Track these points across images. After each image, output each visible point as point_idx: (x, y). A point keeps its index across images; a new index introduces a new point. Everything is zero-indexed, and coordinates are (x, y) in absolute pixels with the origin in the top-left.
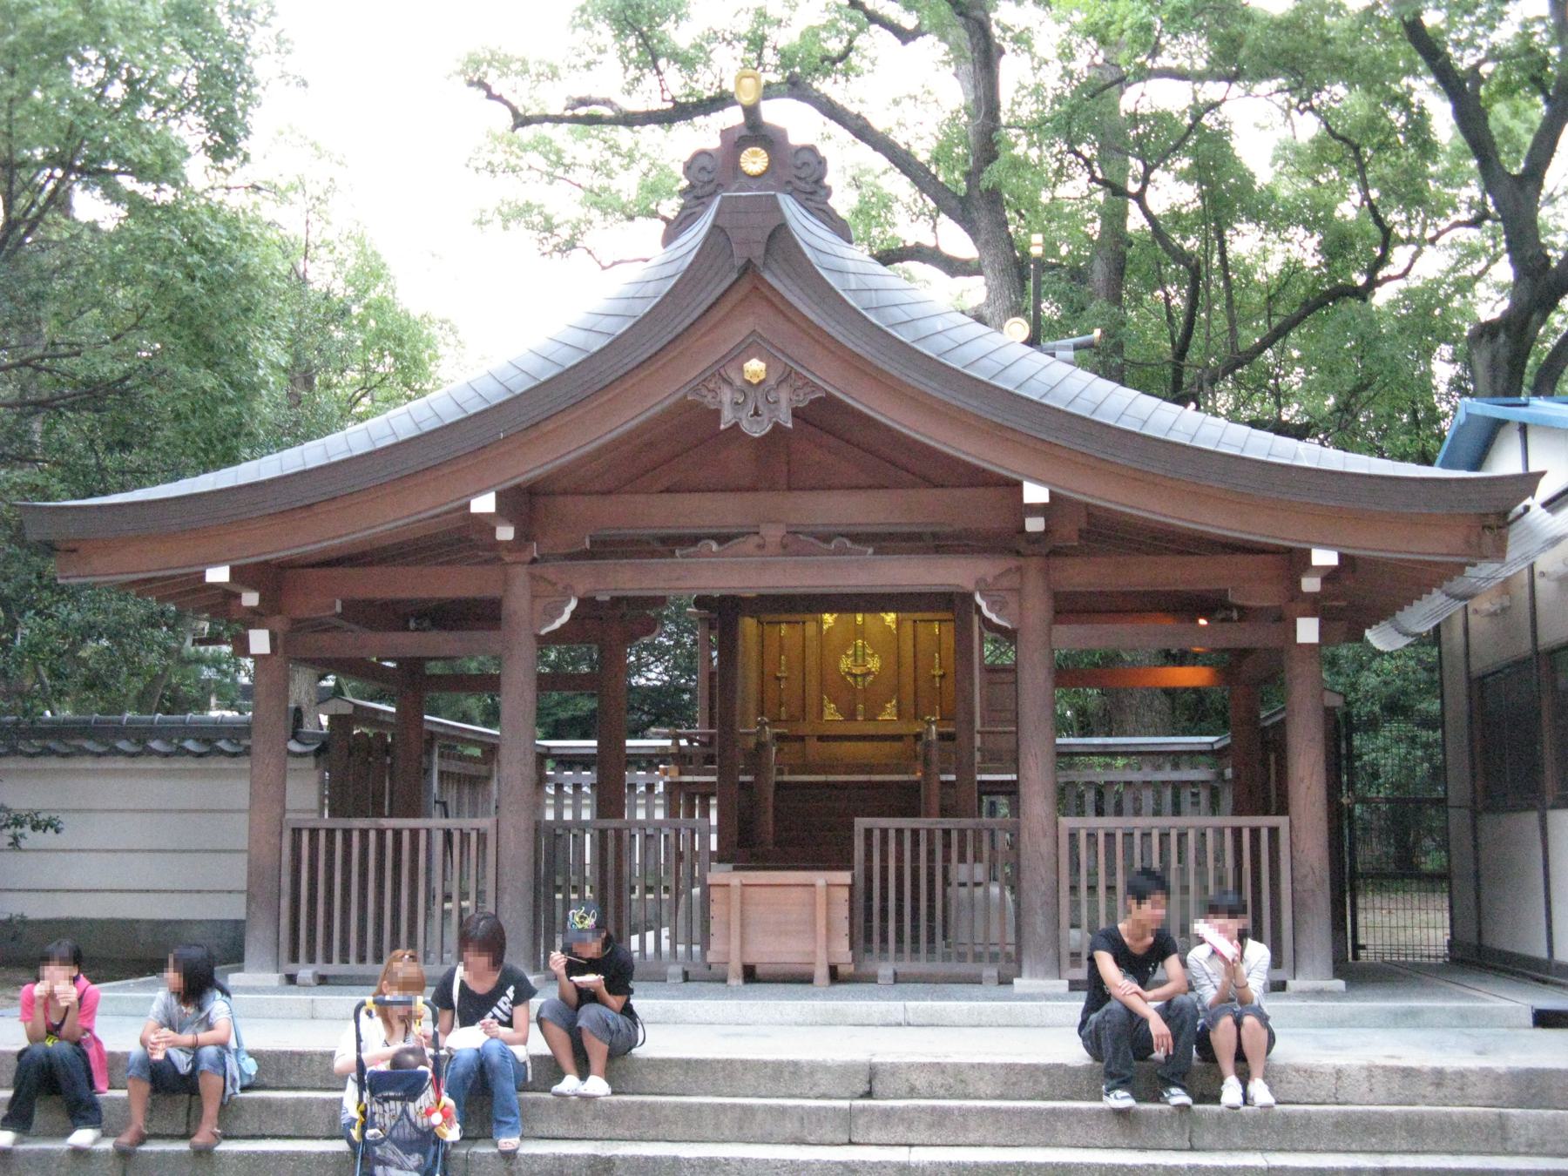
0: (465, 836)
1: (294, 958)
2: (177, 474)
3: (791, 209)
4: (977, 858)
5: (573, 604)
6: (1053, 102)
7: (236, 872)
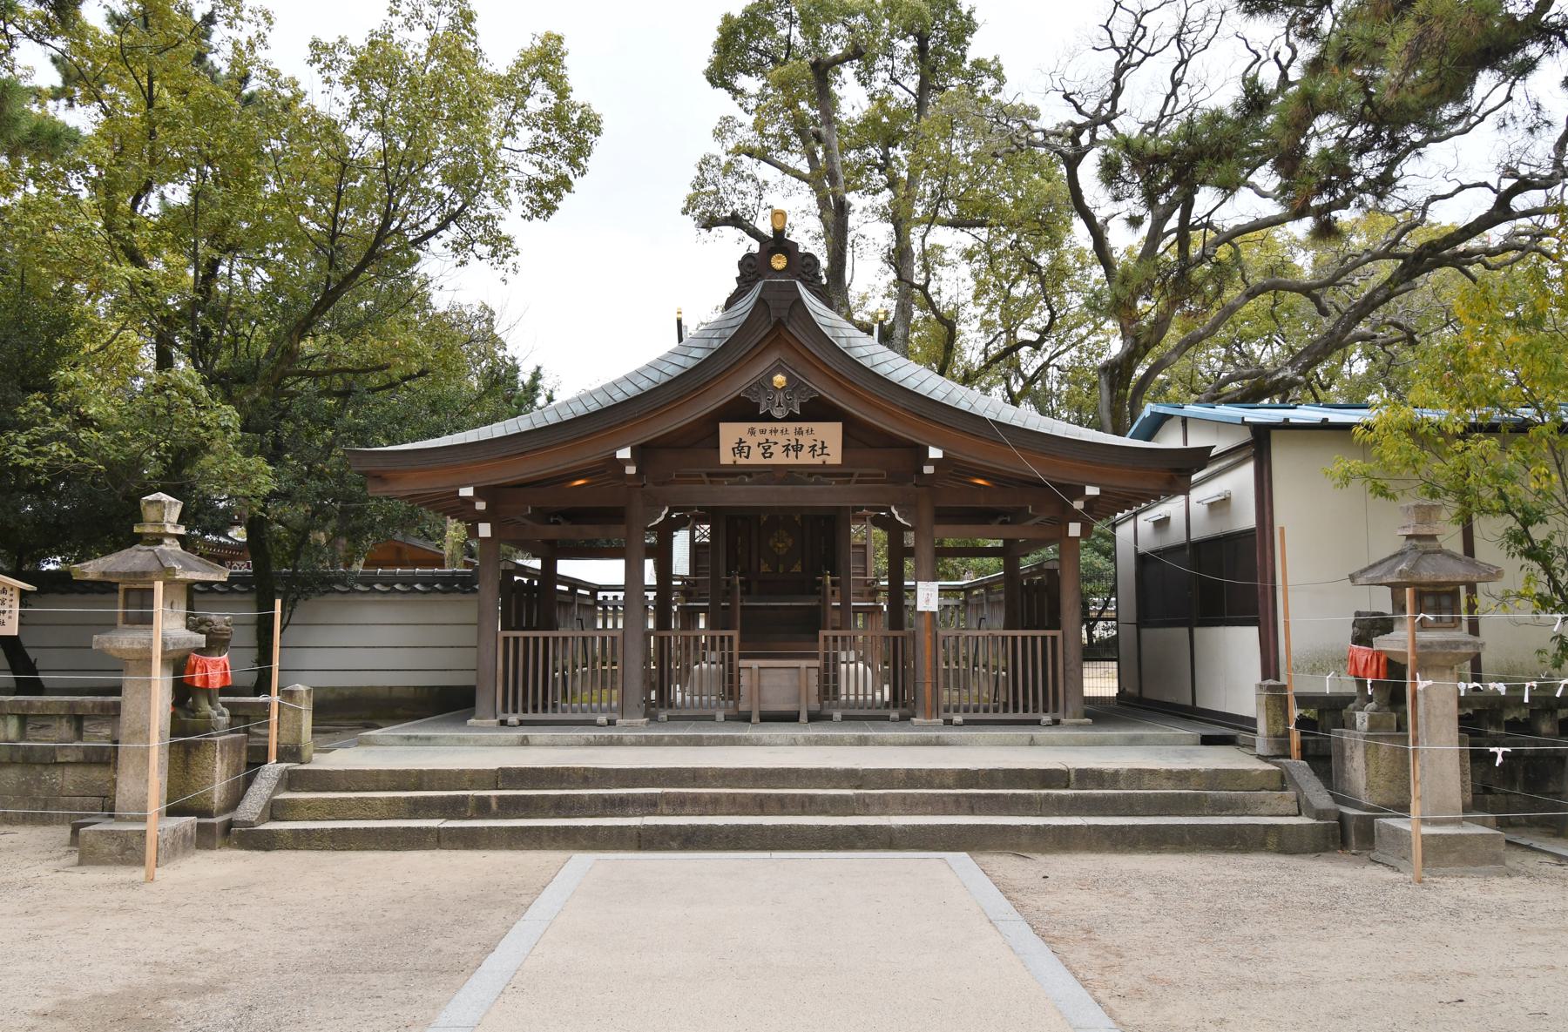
1: (505, 710)
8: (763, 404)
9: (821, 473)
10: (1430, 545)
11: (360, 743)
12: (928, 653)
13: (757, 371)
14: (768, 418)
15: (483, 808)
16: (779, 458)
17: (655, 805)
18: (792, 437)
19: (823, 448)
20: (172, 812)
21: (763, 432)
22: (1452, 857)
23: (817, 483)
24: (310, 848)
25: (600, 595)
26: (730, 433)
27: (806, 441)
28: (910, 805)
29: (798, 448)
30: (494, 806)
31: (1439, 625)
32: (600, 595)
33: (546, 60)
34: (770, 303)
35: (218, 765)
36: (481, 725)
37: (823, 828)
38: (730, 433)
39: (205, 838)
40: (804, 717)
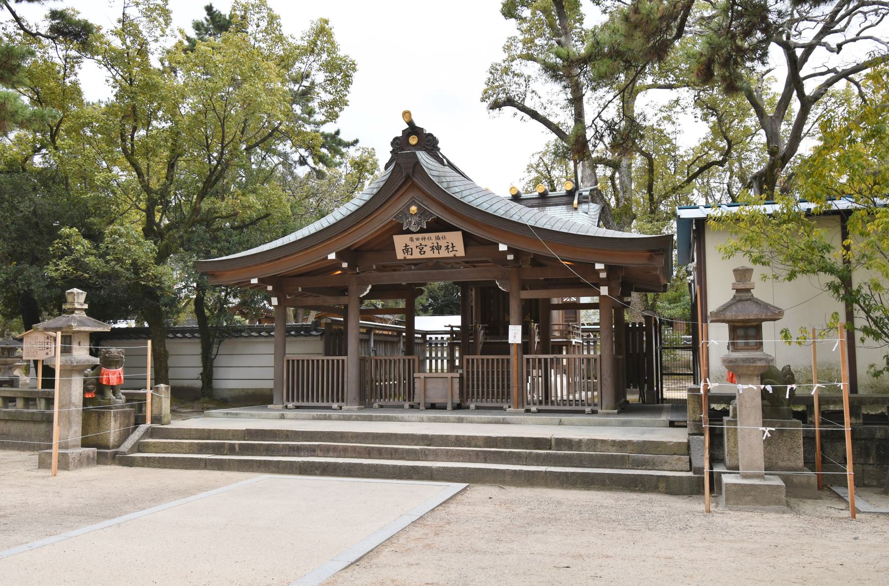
0: (390, 361)
2: (238, 251)
3: (423, 157)
4: (540, 368)
5: (370, 287)
6: (320, 108)
7: (270, 373)
8: (405, 224)
9: (454, 262)
10: (745, 295)
11: (205, 416)
12: (515, 369)
13: (400, 205)
14: (408, 232)
15: (232, 450)
16: (429, 254)
17: (314, 451)
18: (435, 241)
19: (453, 247)
20: (84, 444)
21: (418, 239)
22: (748, 499)
23: (452, 267)
24: (149, 466)
25: (428, 336)
26: (400, 241)
27: (442, 243)
28: (451, 456)
29: (439, 248)
30: (237, 449)
31: (747, 347)
32: (428, 336)
33: (322, 31)
34: (402, 166)
35: (113, 423)
36: (275, 409)
37: (394, 467)
38: (400, 241)
39: (101, 460)
40: (449, 407)
